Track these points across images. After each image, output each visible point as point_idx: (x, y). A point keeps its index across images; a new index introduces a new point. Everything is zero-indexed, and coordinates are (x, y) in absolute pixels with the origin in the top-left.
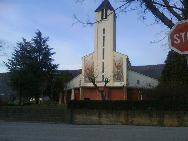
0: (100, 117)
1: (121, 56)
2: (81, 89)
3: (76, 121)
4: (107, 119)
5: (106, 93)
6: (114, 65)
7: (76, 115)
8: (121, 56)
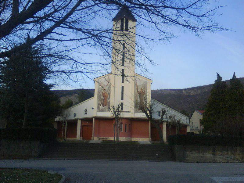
0: (214, 154)
1: (145, 80)
2: (94, 119)
3: (188, 159)
4: (221, 157)
5: (127, 125)
6: (136, 91)
7: (187, 153)
8: (146, 80)
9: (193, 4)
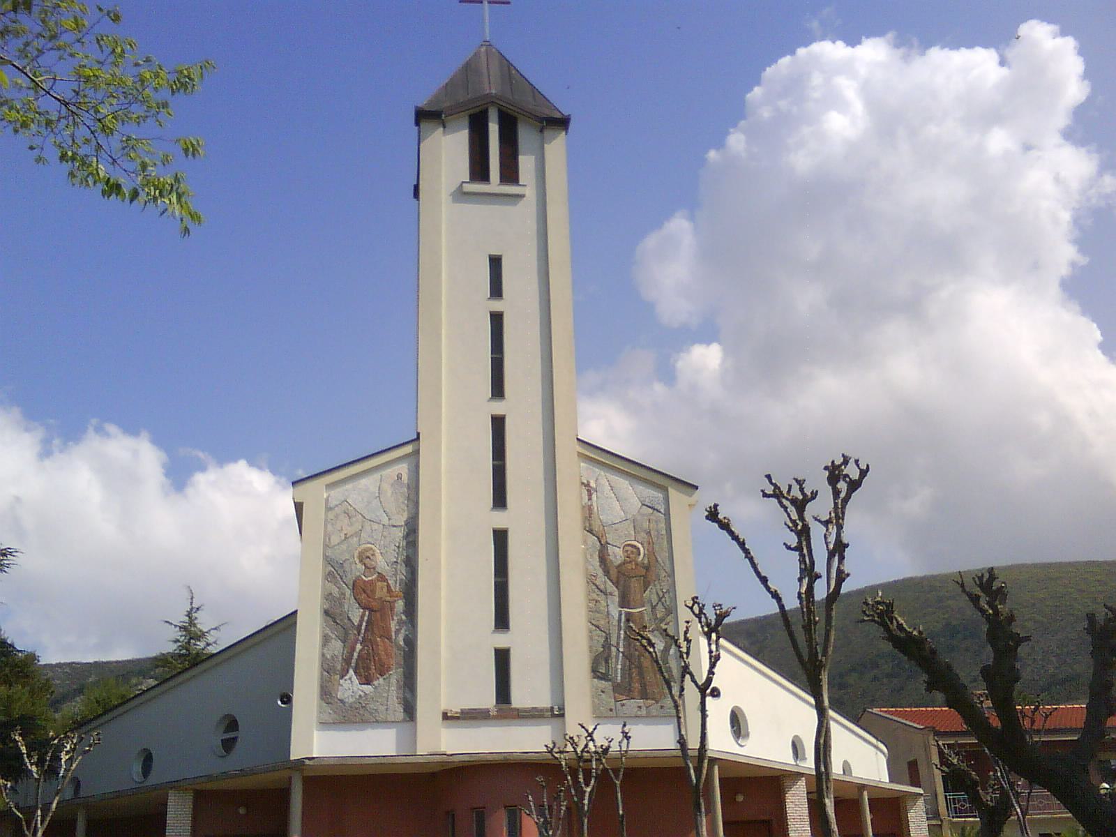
9: (654, 509)
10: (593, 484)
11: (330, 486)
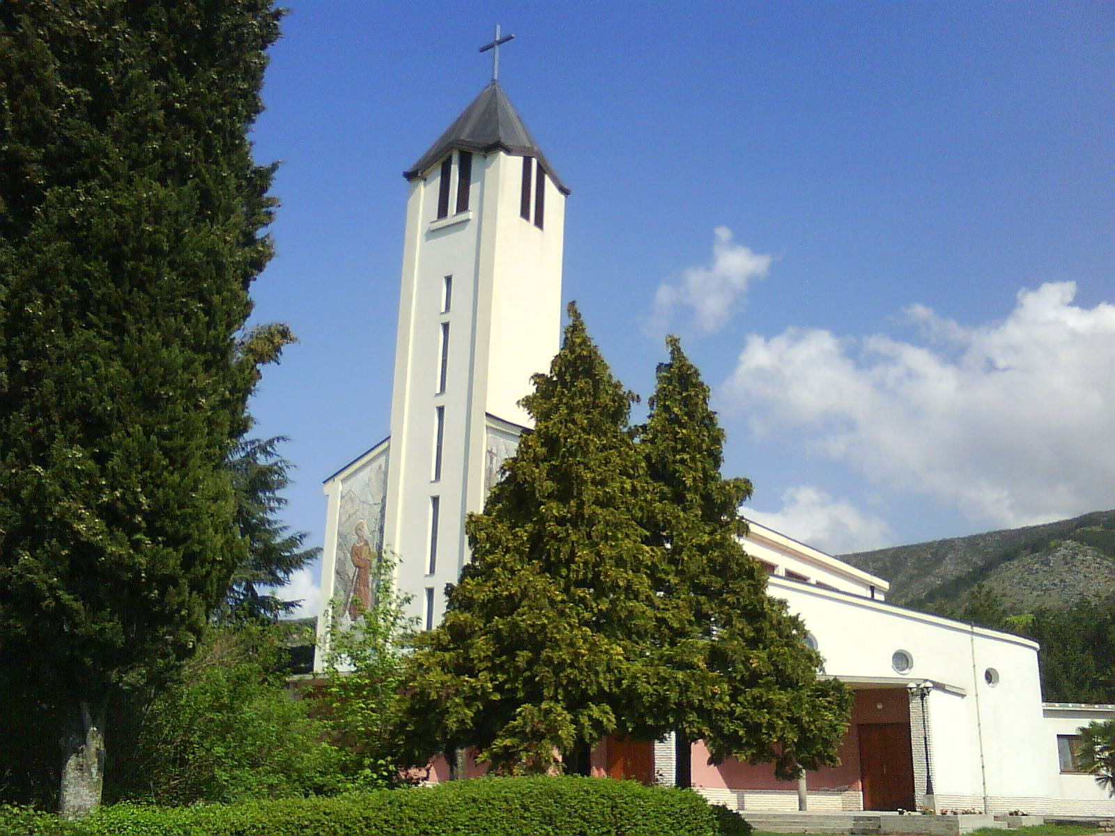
10: (494, 451)
11: (343, 481)
